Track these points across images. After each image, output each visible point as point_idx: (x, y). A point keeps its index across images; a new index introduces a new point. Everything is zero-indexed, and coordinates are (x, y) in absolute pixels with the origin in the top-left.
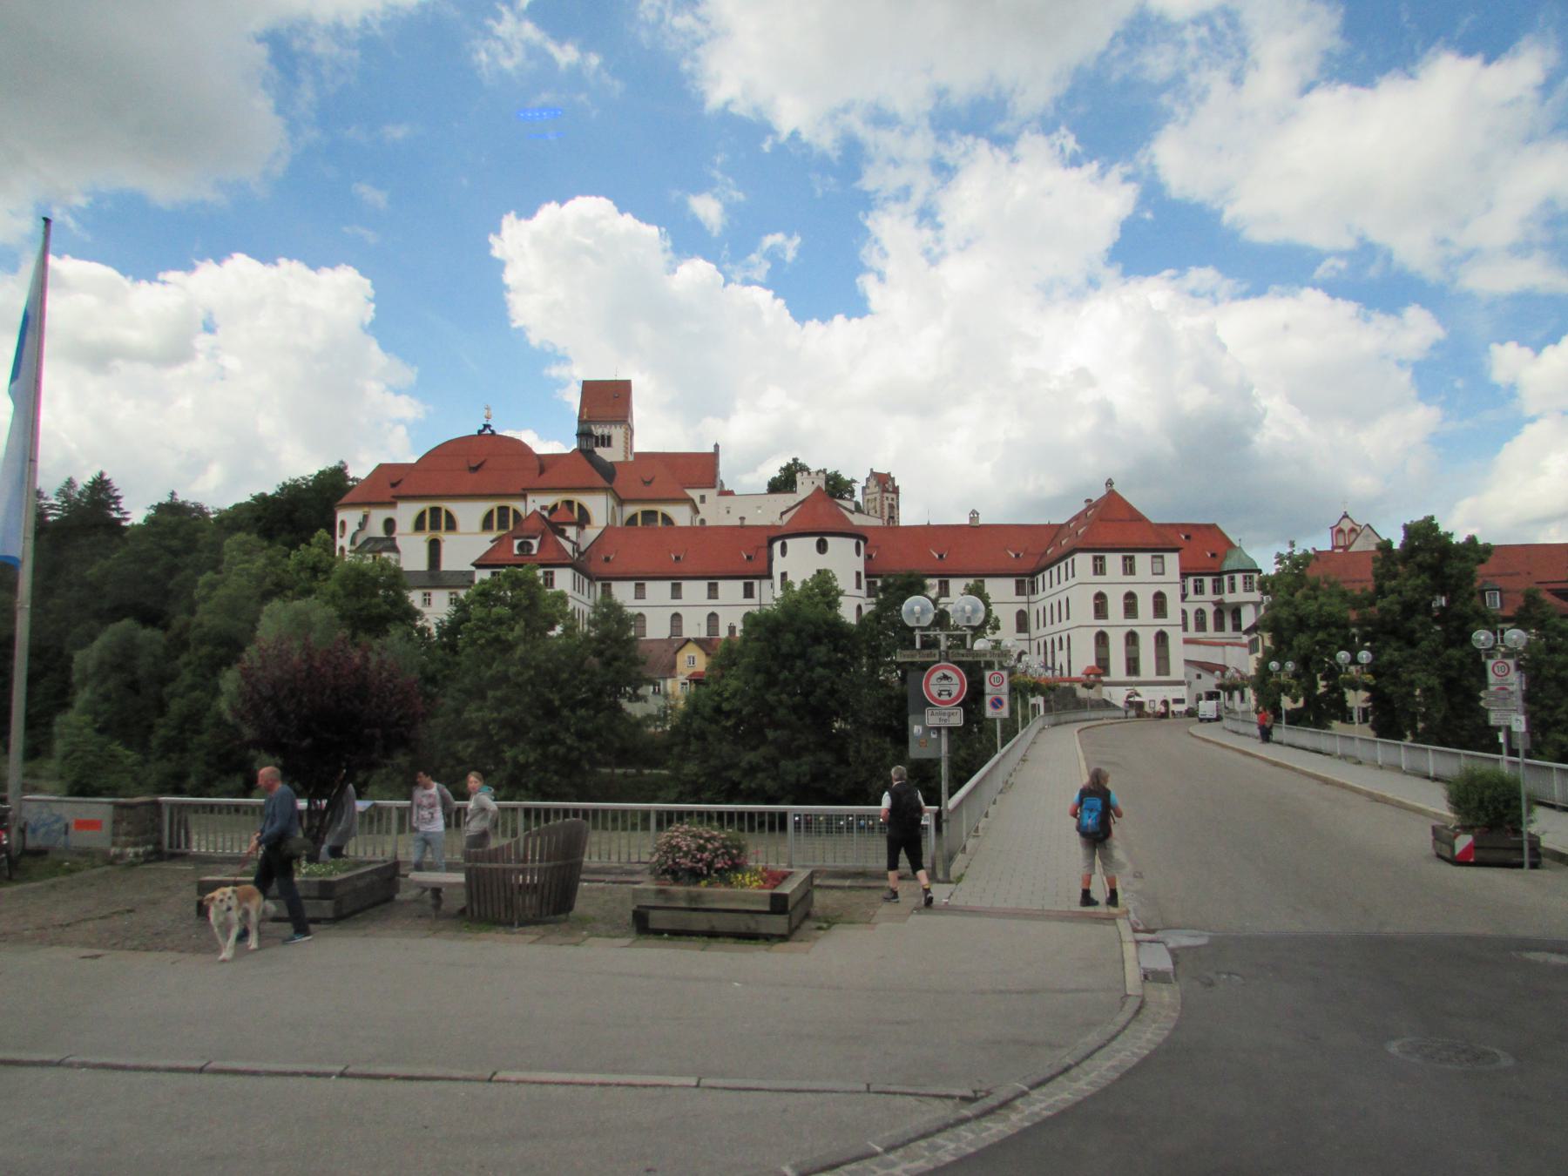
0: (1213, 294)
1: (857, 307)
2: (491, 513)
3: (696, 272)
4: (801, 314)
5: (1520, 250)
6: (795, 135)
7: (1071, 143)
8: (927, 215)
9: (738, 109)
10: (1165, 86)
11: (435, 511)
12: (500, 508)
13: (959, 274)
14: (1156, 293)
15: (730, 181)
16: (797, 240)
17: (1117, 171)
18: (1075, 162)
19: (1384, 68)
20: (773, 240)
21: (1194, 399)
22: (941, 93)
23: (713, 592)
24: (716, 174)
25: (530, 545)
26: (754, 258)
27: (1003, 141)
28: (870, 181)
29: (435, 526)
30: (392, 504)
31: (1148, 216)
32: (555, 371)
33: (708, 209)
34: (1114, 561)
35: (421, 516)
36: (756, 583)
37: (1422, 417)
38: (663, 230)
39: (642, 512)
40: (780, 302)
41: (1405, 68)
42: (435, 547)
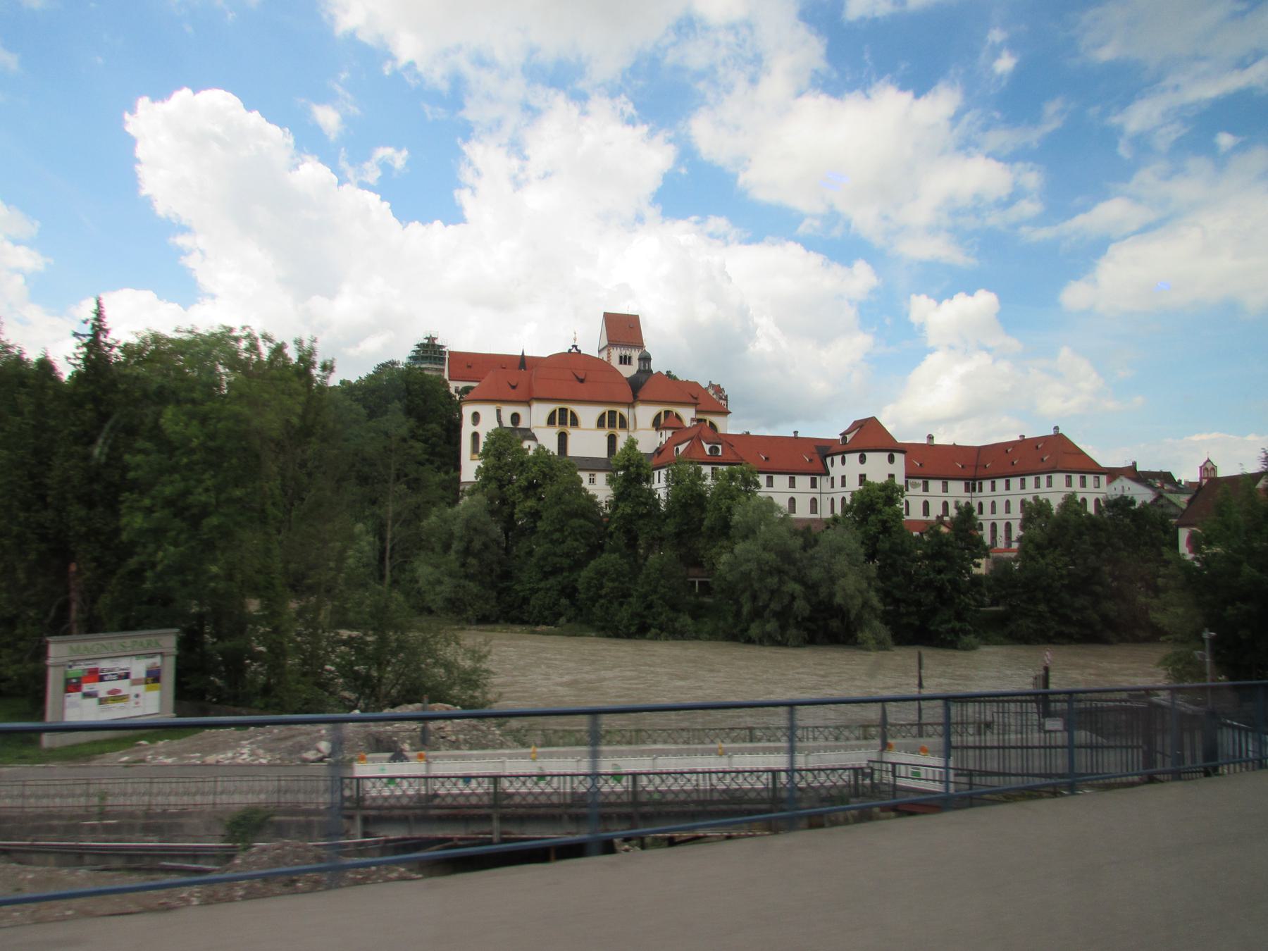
0: (725, 237)
1: (454, 216)
2: (554, 412)
3: (312, 172)
4: (404, 214)
5: (932, 230)
6: (411, 65)
7: (630, 109)
8: (516, 148)
9: (365, 37)
10: (700, 76)
11: (612, 413)
12: (561, 410)
13: (536, 199)
14: (683, 233)
15: (348, 96)
16: (405, 153)
17: (660, 138)
18: (630, 122)
19: (851, 87)
20: (384, 152)
21: (705, 312)
22: (533, 51)
23: (792, 484)
24: (340, 90)
25: (717, 449)
26: (367, 165)
27: (580, 97)
28: (471, 113)
29: (612, 424)
30: (527, 402)
31: (683, 171)
32: (181, 240)
33: (328, 118)
34: (1076, 478)
35: (553, 414)
36: (818, 478)
37: (862, 341)
38: (287, 130)
39: (609, 412)
40: (386, 205)
41: (864, 90)
42: (563, 438)
